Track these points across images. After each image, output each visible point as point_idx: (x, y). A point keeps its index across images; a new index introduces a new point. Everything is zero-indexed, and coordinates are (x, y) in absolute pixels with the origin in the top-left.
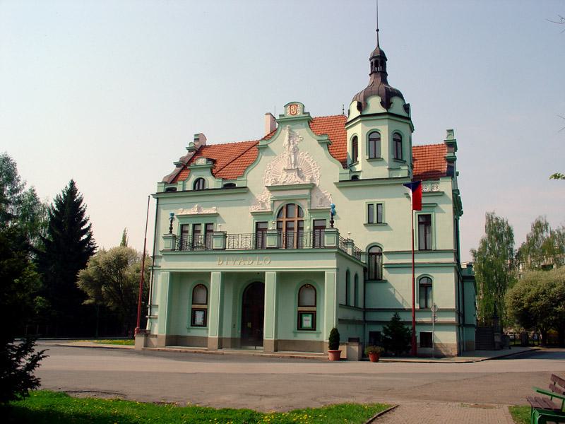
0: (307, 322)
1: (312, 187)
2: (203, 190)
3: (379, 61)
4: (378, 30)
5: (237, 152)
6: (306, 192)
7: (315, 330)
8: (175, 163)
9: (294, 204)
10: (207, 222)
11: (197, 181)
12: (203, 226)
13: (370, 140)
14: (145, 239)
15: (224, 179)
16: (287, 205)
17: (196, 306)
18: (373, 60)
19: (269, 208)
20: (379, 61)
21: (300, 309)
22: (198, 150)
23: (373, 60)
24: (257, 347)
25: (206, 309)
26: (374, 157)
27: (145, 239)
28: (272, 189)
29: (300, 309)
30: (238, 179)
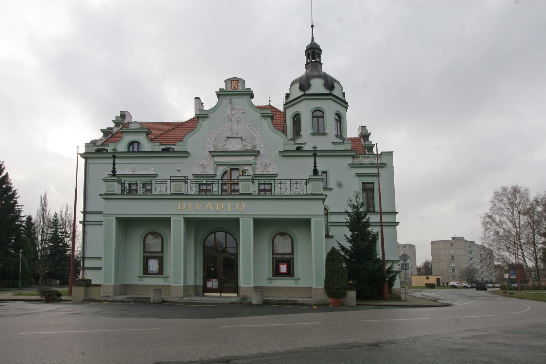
0: (154, 265)
1: (256, 154)
2: (138, 152)
3: (313, 53)
4: (312, 26)
5: (179, 124)
6: (251, 159)
7: (162, 274)
8: (102, 131)
9: (238, 169)
10: (144, 182)
11: (132, 143)
12: (140, 185)
13: (314, 117)
14: (76, 190)
15: (161, 144)
16: (231, 169)
17: (160, 255)
18: (310, 51)
19: (211, 172)
20: (313, 53)
21: (145, 254)
22: (122, 120)
23: (310, 51)
24: (223, 295)
25: (162, 257)
26: (319, 132)
27: (76, 190)
28: (214, 154)
29: (145, 254)
30: (178, 144)
